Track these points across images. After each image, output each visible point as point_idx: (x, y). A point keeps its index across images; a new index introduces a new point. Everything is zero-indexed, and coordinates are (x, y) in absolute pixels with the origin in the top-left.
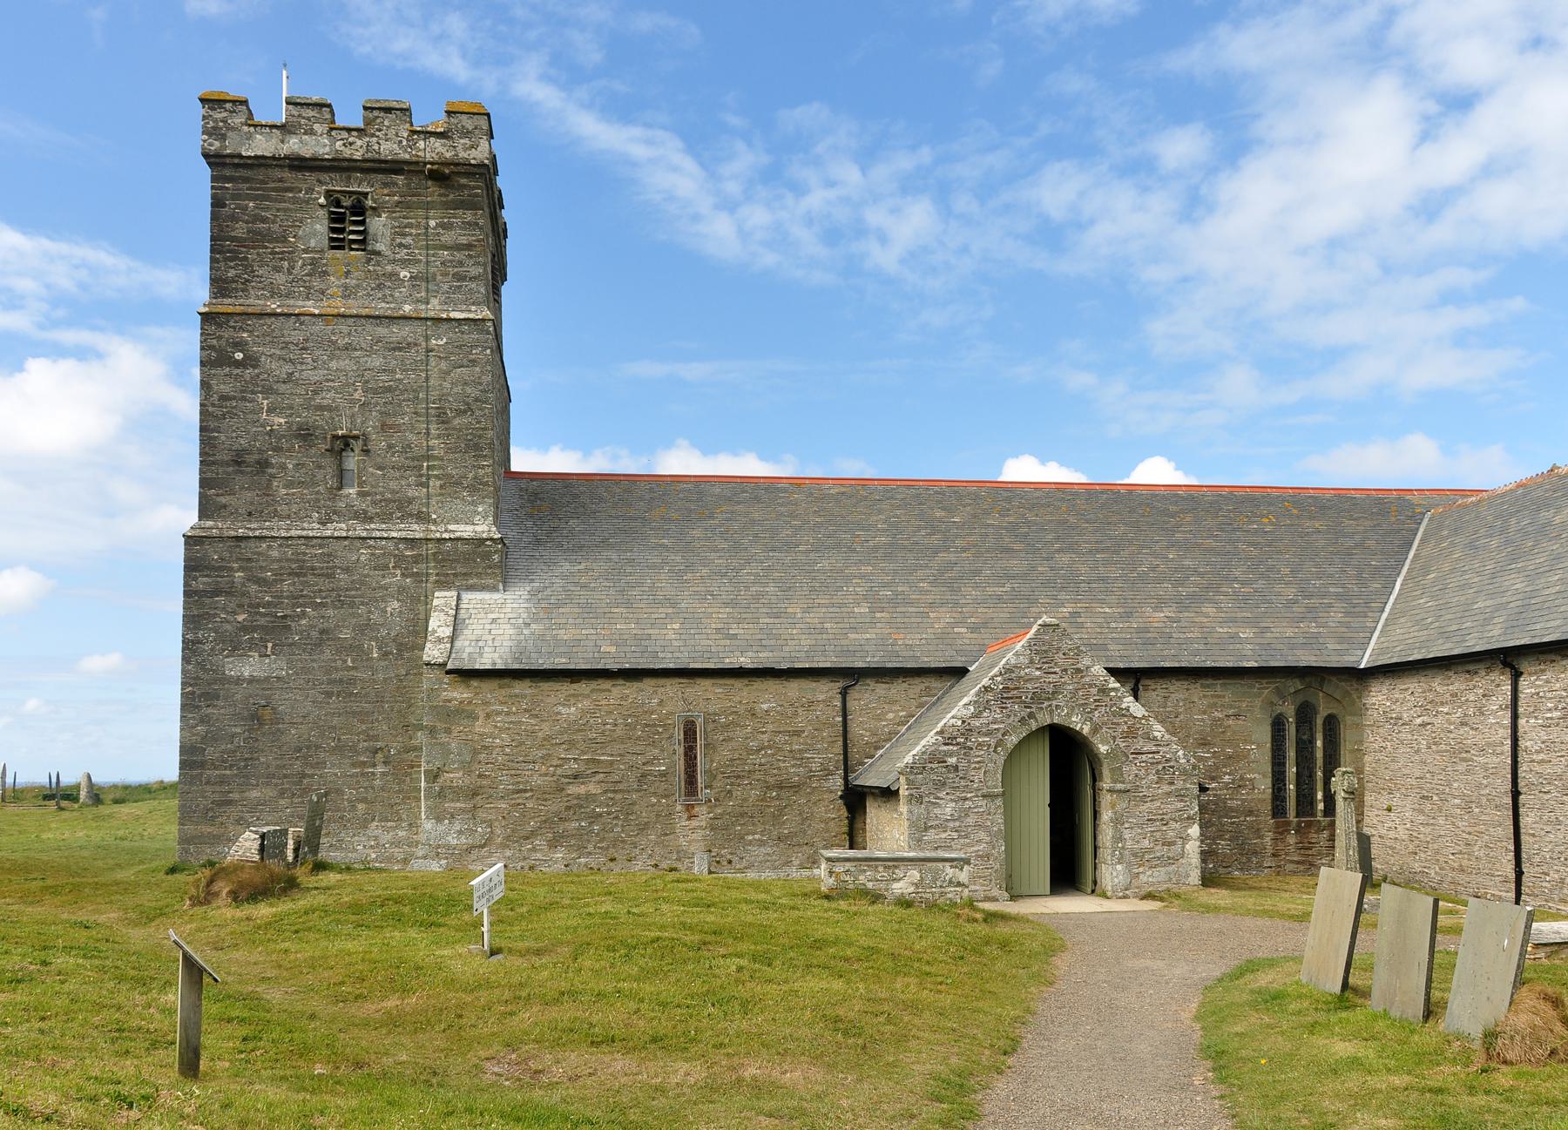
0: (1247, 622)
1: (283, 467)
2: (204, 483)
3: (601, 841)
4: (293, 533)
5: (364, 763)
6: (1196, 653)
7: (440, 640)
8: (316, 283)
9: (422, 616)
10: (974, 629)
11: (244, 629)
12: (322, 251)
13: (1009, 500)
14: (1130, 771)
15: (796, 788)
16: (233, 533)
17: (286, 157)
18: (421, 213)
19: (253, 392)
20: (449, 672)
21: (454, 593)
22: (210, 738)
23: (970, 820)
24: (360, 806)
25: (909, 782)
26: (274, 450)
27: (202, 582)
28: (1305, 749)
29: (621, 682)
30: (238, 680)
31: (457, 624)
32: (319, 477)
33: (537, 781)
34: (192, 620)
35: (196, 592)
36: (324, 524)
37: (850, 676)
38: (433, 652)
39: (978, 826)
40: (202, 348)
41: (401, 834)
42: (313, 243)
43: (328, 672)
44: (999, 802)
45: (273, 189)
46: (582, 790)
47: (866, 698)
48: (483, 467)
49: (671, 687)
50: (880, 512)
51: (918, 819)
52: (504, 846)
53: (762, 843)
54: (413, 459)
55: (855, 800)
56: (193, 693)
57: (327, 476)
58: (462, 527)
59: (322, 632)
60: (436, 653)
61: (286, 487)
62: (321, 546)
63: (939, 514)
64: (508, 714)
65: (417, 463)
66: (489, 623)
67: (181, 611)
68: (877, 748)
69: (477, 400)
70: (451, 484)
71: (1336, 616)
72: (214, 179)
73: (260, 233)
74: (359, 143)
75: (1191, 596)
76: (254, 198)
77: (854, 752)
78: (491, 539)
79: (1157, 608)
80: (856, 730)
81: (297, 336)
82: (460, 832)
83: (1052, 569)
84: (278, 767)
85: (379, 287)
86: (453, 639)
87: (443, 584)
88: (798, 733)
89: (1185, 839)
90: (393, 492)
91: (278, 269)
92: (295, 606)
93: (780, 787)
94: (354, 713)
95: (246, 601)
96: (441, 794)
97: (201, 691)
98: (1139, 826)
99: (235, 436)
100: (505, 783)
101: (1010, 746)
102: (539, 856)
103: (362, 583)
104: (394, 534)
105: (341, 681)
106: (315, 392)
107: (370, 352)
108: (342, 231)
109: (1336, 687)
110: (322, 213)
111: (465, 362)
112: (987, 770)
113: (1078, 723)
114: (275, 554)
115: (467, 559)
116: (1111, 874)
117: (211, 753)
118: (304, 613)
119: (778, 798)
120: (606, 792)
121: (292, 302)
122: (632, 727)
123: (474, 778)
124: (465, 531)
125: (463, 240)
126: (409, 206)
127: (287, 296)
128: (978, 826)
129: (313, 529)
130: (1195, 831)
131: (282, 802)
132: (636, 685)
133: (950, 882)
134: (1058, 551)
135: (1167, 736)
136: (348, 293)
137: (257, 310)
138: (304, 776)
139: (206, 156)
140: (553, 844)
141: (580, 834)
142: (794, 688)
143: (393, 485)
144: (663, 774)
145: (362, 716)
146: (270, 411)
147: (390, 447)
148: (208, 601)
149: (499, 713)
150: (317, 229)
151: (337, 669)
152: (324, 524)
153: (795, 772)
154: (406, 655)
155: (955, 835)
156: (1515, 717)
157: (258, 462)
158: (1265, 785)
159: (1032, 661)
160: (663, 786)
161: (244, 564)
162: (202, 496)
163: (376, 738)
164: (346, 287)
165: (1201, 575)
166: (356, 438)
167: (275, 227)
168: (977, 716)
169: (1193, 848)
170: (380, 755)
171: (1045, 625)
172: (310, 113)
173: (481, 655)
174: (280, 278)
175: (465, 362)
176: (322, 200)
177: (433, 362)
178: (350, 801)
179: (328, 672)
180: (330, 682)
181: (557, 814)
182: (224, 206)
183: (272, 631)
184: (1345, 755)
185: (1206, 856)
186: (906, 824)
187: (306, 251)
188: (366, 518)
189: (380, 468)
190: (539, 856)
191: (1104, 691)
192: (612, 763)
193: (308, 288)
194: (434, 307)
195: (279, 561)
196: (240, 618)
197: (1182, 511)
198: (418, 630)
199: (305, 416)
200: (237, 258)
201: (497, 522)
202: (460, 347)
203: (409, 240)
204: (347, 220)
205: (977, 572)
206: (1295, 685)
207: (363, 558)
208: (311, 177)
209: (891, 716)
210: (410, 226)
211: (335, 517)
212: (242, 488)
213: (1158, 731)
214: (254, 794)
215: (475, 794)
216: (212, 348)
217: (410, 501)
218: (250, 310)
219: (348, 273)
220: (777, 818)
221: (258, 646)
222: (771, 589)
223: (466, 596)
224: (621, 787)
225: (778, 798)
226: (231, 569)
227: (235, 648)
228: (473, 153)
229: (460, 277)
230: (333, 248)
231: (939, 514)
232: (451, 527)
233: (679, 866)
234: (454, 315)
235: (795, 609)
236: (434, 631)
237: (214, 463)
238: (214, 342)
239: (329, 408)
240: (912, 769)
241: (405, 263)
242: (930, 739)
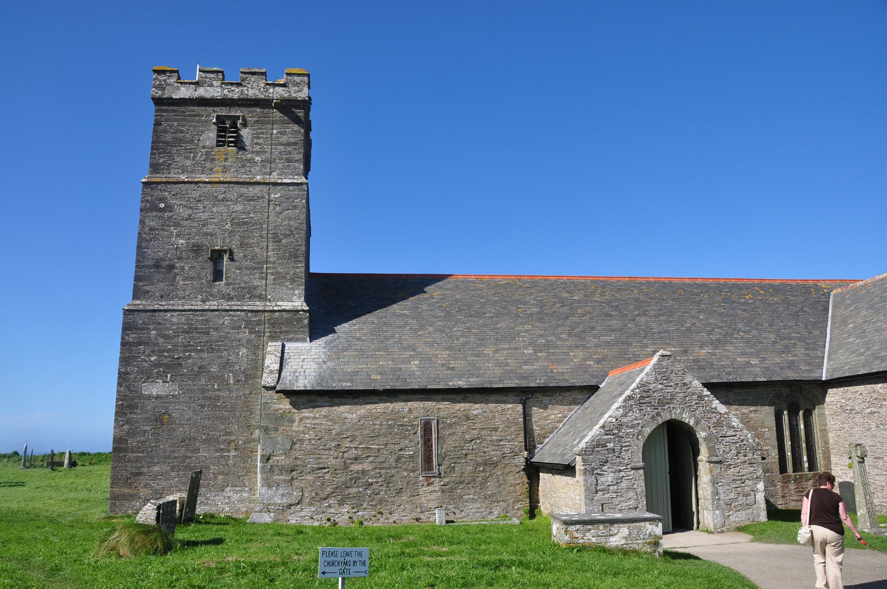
0: (751, 355)
1: (182, 268)
2: (137, 278)
3: (372, 501)
4: (186, 307)
5: (223, 449)
6: (729, 374)
7: (272, 372)
8: (208, 165)
9: (260, 357)
10: (598, 362)
11: (156, 365)
12: (213, 147)
13: (603, 287)
15: (495, 465)
16: (151, 308)
17: (197, 98)
18: (269, 126)
19: (168, 226)
20: (277, 392)
21: (280, 343)
22: (131, 433)
23: (624, 485)
24: (220, 477)
25: (584, 460)
26: (178, 259)
27: (132, 337)
29: (384, 398)
30: (149, 397)
32: (203, 274)
33: (332, 462)
34: (125, 360)
35: (128, 343)
36: (204, 301)
37: (526, 395)
39: (629, 489)
40: (142, 202)
41: (245, 495)
42: (207, 143)
43: (203, 392)
44: (641, 472)
45: (189, 116)
46: (359, 467)
48: (299, 267)
50: (531, 294)
51: (591, 485)
52: (311, 504)
53: (474, 501)
54: (258, 263)
55: (533, 471)
56: (122, 405)
57: (208, 272)
58: (285, 303)
59: (200, 367)
60: (269, 380)
61: (184, 280)
62: (202, 315)
63: (565, 295)
64: (314, 418)
65: (258, 266)
67: (118, 355)
68: (545, 438)
69: (296, 228)
70: (280, 278)
71: (800, 351)
72: (157, 111)
73: (179, 139)
74: (237, 90)
75: (718, 340)
76: (178, 121)
78: (303, 311)
79: (701, 348)
81: (196, 194)
82: (283, 495)
83: (636, 326)
84: (171, 452)
85: (243, 166)
86: (280, 371)
87: (273, 338)
90: (245, 283)
91: (187, 158)
92: (185, 351)
93: (485, 464)
94: (217, 418)
95: (156, 348)
96: (271, 470)
97: (127, 405)
99: (155, 251)
100: (312, 464)
101: (646, 435)
102: (332, 510)
103: (226, 338)
104: (245, 308)
105: (210, 397)
106: (204, 225)
107: (236, 202)
108: (224, 137)
110: (214, 127)
111: (290, 207)
112: (635, 454)
114: (175, 320)
115: (289, 322)
117: (132, 442)
118: (190, 356)
119: (484, 471)
120: (374, 469)
121: (194, 175)
122: (391, 427)
123: (291, 460)
124: (288, 305)
125: (292, 140)
126: (262, 123)
127: (192, 172)
128: (629, 489)
130: (761, 486)
131: (172, 474)
133: (650, 535)
134: (637, 316)
135: (740, 425)
136: (225, 170)
137: (174, 180)
138: (187, 457)
139: (154, 99)
140: (341, 503)
141: (358, 496)
143: (246, 278)
144: (411, 457)
145: (223, 419)
146: (177, 236)
147: (245, 256)
148: (134, 348)
149: (308, 418)
150: (211, 135)
151: (208, 390)
152: (204, 301)
153: (495, 455)
154: (250, 382)
155: (614, 495)
157: (169, 266)
159: (656, 379)
160: (411, 464)
161: (157, 326)
162: (135, 286)
163: (230, 434)
164: (224, 167)
165: (720, 328)
166: (225, 251)
167: (188, 136)
168: (625, 415)
169: (760, 497)
170: (232, 445)
171: (663, 356)
172: (211, 75)
173: (297, 381)
174: (188, 163)
175: (290, 207)
176: (214, 120)
177: (271, 207)
178: (214, 474)
179: (203, 392)
180: (205, 398)
181: (345, 483)
182: (161, 125)
183: (170, 368)
186: (583, 488)
187: (204, 147)
188: (230, 299)
189: (238, 269)
190: (332, 510)
191: (701, 397)
192: (379, 450)
193: (203, 168)
194: (274, 177)
195: (178, 324)
196: (153, 359)
197: (701, 292)
198: (257, 366)
200: (165, 152)
201: (307, 301)
202: (287, 199)
203: (261, 141)
204: (228, 133)
205: (593, 328)
207: (226, 322)
208: (210, 109)
209: (553, 417)
210: (263, 133)
211: (211, 298)
212: (158, 281)
214: (156, 468)
215: (292, 471)
216: (147, 201)
217: (255, 288)
218: (170, 180)
219: (226, 159)
220: (483, 484)
221: (162, 376)
222: (472, 339)
223: (288, 345)
224: (385, 465)
225: (484, 471)
226: (149, 329)
227: (149, 377)
228: (300, 94)
229: (289, 160)
230: (218, 146)
231: (565, 295)
232: (279, 303)
233: (422, 516)
234: (285, 181)
235: (489, 351)
236: (268, 367)
237: (143, 266)
238: (149, 198)
239: (211, 235)
240: (584, 453)
241: (258, 153)
242: (596, 430)
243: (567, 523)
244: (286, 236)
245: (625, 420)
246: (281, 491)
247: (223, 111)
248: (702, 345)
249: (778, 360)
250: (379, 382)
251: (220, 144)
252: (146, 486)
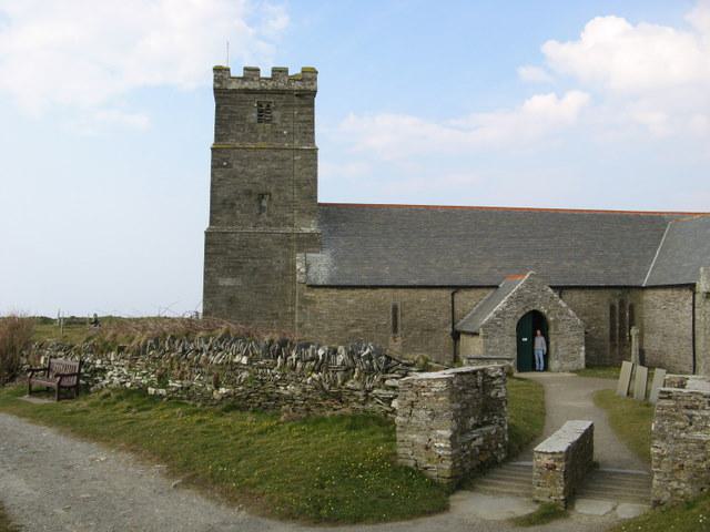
10: (500, 270)
14: (560, 326)
28: (622, 316)
30: (224, 286)
31: (307, 267)
34: (207, 264)
37: (456, 288)
38: (299, 278)
46: (354, 331)
47: (461, 296)
49: (388, 292)
55: (456, 335)
57: (256, 210)
66: (319, 265)
70: (302, 212)
77: (456, 318)
80: (457, 309)
87: (299, 251)
88: (435, 310)
89: (580, 351)
91: (239, 131)
97: (210, 290)
98: (567, 342)
109: (635, 293)
112: (511, 326)
113: (543, 310)
116: (554, 364)
124: (308, 230)
130: (583, 348)
132: (375, 291)
142: (434, 292)
156: (694, 308)
158: (607, 331)
169: (582, 354)
174: (239, 134)
184: (637, 319)
185: (586, 356)
199: (249, 187)
201: (320, 224)
204: (264, 114)
206: (618, 292)
208: (252, 96)
213: (571, 312)
223: (308, 255)
240: (484, 327)
241: (285, 128)
243: (469, 359)
246: (675, 332)
248: (569, 259)
249: (617, 271)
250: (365, 280)
251: (260, 121)
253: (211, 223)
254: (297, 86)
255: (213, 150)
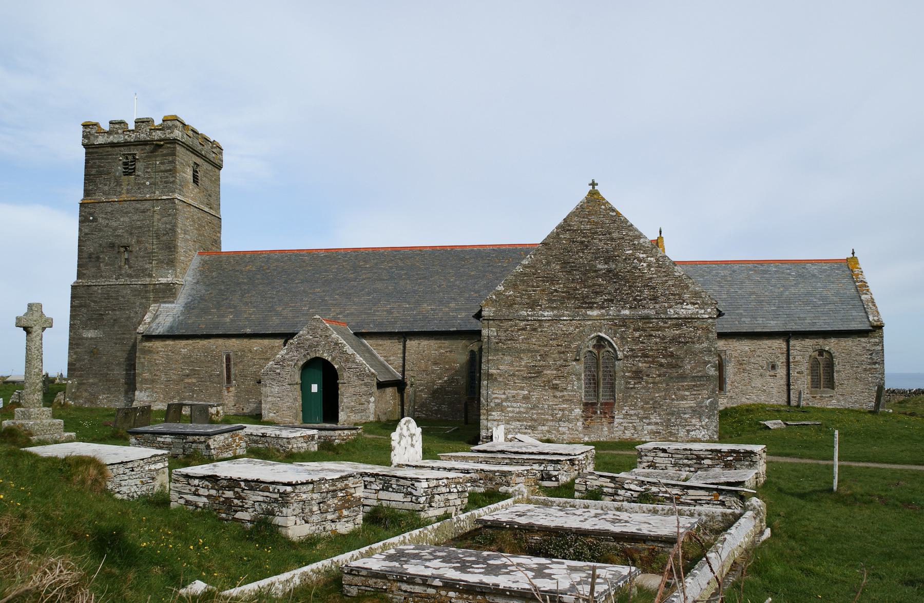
22: (78, 360)
30: (87, 339)
38: (141, 329)
49: (220, 341)
81: (109, 209)
87: (155, 301)
91: (105, 185)
113: (326, 356)
115: (164, 291)
117: (78, 365)
129: (113, 281)
143: (141, 264)
144: (218, 375)
172: (117, 126)
174: (106, 188)
217: (146, 269)
241: (148, 179)
244: (164, 235)
245: (287, 357)
247: (125, 151)
252: (86, 390)
253: (80, 275)
254: (157, 135)
255: (82, 205)
